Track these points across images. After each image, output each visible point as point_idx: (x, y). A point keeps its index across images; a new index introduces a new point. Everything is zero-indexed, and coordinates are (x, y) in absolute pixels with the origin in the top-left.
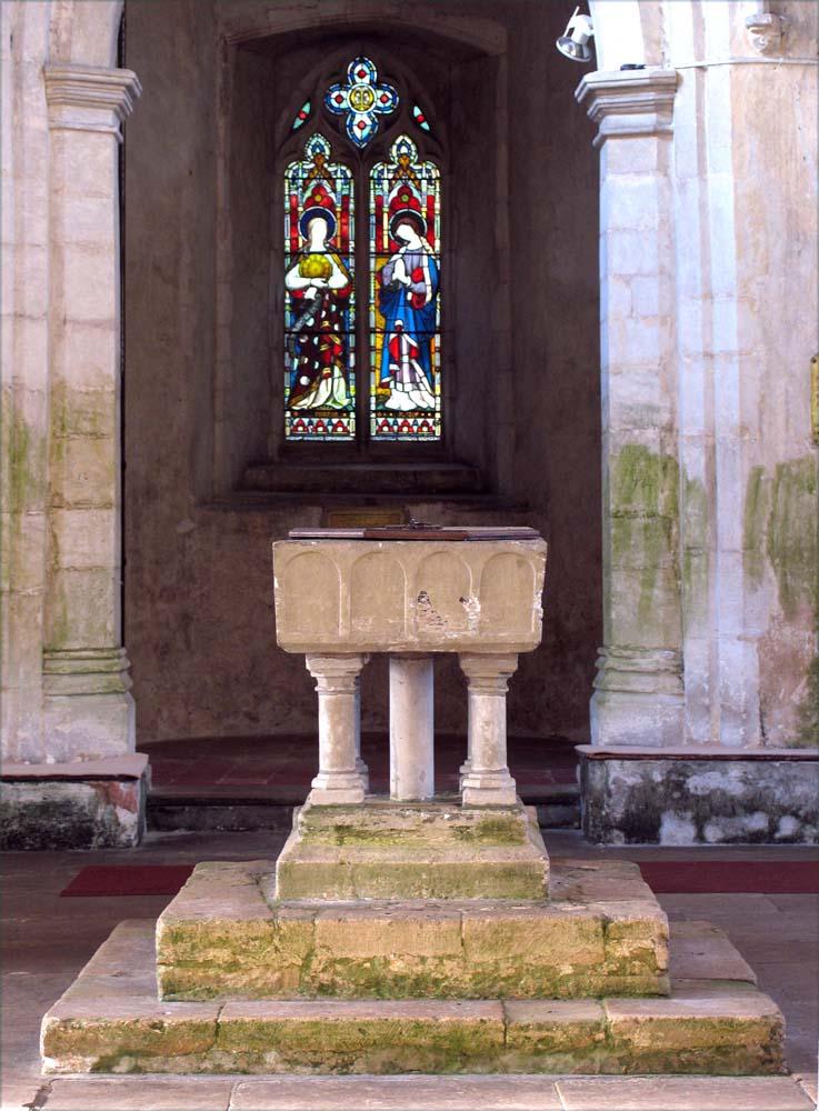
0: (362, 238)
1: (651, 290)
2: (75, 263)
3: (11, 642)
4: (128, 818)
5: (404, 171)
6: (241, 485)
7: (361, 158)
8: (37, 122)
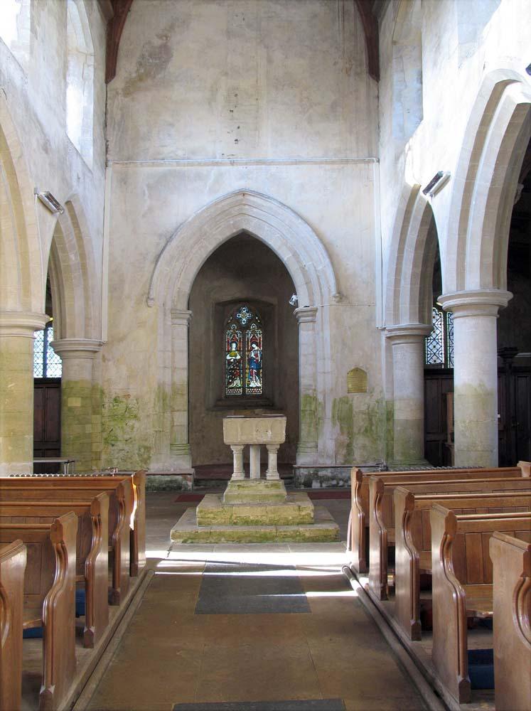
0: (244, 348)
4: (190, 484)
5: (254, 332)
7: (244, 329)
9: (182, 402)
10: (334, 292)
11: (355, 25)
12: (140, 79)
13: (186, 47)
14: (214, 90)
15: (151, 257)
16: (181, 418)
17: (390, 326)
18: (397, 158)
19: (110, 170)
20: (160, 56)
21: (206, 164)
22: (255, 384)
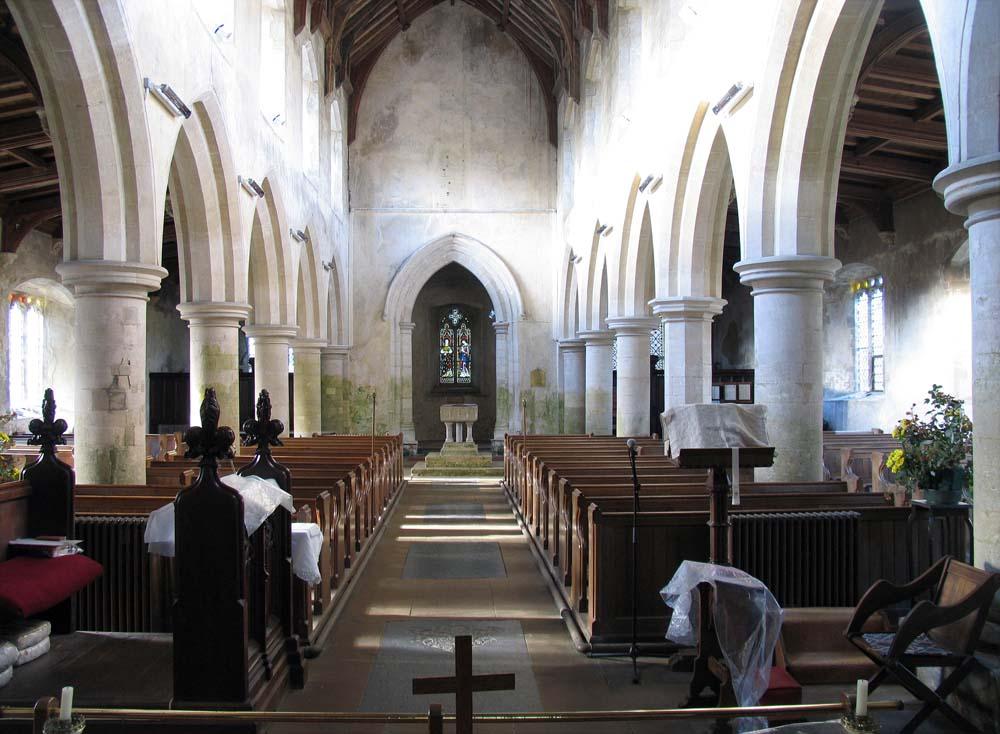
0: (455, 343)
1: (504, 361)
2: (405, 357)
3: (844, 395)
4: (415, 451)
5: (463, 331)
6: (432, 392)
7: (455, 328)
8: (398, 332)
9: (408, 391)
10: (521, 312)
11: (539, 101)
12: (374, 141)
13: (409, 117)
14: (430, 153)
15: (384, 284)
16: (408, 404)
17: (561, 339)
18: (564, 220)
19: (352, 214)
20: (389, 123)
21: (426, 212)
22: (465, 374)
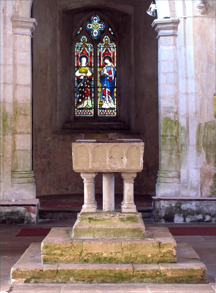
0: (95, 63)
1: (172, 76)
2: (20, 69)
4: (34, 216)
5: (107, 45)
6: (63, 128)
7: (95, 42)
8: (10, 32)
